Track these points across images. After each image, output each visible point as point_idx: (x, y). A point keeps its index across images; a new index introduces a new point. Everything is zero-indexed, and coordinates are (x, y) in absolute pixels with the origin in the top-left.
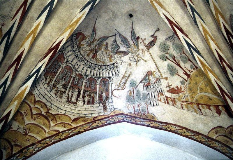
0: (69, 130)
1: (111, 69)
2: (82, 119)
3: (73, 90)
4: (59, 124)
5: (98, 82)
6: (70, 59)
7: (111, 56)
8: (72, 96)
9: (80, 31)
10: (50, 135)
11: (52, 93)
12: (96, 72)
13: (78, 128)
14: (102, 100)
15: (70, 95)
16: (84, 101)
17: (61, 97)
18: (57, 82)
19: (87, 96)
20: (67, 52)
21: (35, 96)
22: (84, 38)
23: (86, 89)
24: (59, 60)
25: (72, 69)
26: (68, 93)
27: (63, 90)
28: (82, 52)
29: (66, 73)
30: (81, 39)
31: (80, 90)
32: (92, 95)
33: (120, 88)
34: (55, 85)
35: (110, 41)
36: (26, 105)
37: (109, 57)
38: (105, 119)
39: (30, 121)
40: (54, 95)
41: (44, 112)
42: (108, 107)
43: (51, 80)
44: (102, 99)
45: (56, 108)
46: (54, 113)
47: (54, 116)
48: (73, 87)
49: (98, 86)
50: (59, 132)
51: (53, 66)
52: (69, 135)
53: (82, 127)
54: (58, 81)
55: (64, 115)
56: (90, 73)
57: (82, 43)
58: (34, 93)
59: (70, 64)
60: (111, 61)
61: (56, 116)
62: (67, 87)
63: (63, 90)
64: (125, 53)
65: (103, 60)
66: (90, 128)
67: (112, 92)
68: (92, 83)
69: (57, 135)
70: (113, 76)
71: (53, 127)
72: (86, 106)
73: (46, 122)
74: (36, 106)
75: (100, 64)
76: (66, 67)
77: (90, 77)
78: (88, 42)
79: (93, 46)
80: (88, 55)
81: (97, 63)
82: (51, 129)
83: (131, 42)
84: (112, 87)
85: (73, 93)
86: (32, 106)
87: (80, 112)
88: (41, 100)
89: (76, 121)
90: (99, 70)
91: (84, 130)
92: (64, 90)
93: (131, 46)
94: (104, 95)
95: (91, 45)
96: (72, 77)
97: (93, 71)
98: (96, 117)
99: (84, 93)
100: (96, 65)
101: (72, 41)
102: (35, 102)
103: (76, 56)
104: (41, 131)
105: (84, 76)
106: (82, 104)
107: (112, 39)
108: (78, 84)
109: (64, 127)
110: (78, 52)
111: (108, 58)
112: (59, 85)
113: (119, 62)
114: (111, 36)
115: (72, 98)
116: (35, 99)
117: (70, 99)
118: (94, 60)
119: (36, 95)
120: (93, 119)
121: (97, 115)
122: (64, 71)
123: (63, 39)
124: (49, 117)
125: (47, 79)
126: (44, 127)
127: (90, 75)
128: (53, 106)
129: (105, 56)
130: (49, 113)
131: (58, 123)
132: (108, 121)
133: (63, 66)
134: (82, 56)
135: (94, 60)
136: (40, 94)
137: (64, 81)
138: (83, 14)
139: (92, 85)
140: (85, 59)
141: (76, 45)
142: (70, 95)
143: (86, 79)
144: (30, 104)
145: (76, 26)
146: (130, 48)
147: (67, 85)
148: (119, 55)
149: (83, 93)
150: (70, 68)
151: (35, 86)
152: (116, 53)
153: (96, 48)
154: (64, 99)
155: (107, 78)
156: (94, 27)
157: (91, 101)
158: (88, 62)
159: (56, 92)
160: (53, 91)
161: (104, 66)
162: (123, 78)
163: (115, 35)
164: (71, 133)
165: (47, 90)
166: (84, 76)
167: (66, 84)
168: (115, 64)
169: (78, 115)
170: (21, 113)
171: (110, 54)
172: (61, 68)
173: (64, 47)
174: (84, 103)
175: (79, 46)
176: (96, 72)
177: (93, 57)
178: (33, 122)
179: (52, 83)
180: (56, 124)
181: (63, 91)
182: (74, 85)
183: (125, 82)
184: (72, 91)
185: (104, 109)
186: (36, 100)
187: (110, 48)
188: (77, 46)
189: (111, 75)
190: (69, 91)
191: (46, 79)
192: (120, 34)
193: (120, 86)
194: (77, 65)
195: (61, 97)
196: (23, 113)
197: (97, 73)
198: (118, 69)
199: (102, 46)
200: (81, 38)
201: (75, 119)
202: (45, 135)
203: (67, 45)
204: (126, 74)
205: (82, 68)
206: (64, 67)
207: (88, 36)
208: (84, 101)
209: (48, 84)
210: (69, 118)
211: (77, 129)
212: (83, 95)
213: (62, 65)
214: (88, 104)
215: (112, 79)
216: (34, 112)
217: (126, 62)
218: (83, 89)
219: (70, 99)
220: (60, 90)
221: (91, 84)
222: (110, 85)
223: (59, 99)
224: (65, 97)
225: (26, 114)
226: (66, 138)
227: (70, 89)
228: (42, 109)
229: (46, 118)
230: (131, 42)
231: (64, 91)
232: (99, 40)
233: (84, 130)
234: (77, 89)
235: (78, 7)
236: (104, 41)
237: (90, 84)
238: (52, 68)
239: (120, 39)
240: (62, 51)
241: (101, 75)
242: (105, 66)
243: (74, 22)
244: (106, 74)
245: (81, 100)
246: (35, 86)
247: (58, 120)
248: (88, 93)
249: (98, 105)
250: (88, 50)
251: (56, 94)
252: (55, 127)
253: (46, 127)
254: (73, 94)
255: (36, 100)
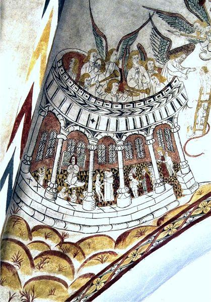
0: (112, 265)
1: (167, 98)
2: (134, 233)
3: (101, 176)
4: (90, 258)
5: (148, 138)
6: (72, 116)
7: (160, 69)
8: (103, 191)
9: (64, 52)
10: (77, 290)
11: (58, 201)
12: (137, 118)
13: (130, 255)
14: (168, 175)
15: (98, 190)
16: (130, 192)
17: (81, 201)
18: (63, 173)
19: (134, 177)
20: (58, 105)
21: (25, 222)
22: (82, 60)
23: (128, 163)
24: (49, 130)
25: (86, 135)
26: (93, 186)
27: (81, 184)
28: (92, 90)
29: (75, 148)
30: (77, 66)
31: (115, 170)
32: (144, 171)
33: (199, 133)
34: (60, 182)
35: (144, 38)
36: (13, 244)
37: (155, 75)
38: (182, 216)
39: (31, 274)
40: (65, 203)
41: (53, 245)
42: (183, 186)
43: (48, 175)
44: (167, 173)
45: (77, 228)
46: (75, 241)
47: (76, 245)
48: (99, 171)
49: (151, 148)
50: (93, 277)
51: (41, 147)
52: (113, 278)
53: (137, 250)
54: (65, 171)
55: (96, 236)
56: (127, 125)
57: (83, 72)
58: (22, 214)
59: (76, 125)
60: (162, 80)
61: (81, 245)
62: (87, 176)
63: (81, 184)
64: (187, 49)
65: (145, 85)
66: (152, 248)
67: (184, 149)
68: (137, 146)
69: (89, 284)
70: (175, 112)
71: (79, 270)
72: (138, 200)
73: (64, 263)
74: (34, 239)
75: (143, 96)
76: (71, 137)
77: (128, 135)
78: (95, 63)
79: (111, 67)
80: (108, 90)
81: (135, 99)
82: (76, 276)
83: (192, 18)
84: (182, 136)
85: (102, 182)
86: (26, 242)
87: (128, 219)
88: (42, 224)
89: (124, 240)
90: (144, 110)
91: (141, 256)
92: (84, 183)
93: (195, 26)
94: (169, 162)
95: (106, 67)
96: (90, 150)
97: (130, 119)
98: (162, 219)
99: (126, 173)
100: (133, 103)
101: (59, 78)
102: (31, 232)
103: (81, 104)
104: (59, 286)
105: (115, 138)
106: (129, 200)
107: (148, 29)
108: (107, 161)
109: (102, 262)
110: (81, 94)
111: (153, 77)
112: (70, 176)
113: (178, 74)
114: (141, 27)
115: (104, 194)
116: (28, 226)
117: (101, 198)
118: (125, 95)
119: (26, 217)
120: (158, 224)
121: (164, 211)
122: (68, 145)
123: (33, 86)
124: (68, 250)
125: (38, 177)
126: (61, 276)
127: (127, 129)
128: (69, 227)
129: (146, 74)
130: (66, 243)
131: (87, 257)
132: (188, 217)
133: (63, 136)
134: (96, 98)
135: (125, 95)
136: (36, 212)
137: (76, 166)
138: (51, 16)
139: (138, 150)
140: (103, 101)
141: (72, 83)
142: (98, 190)
143: (121, 143)
144: (21, 240)
145: (47, 48)
146: (193, 32)
147: (86, 172)
148: (177, 59)
149: (124, 174)
150: (79, 134)
151: (18, 201)
152: (168, 58)
153: (120, 66)
154: (89, 203)
155: (166, 122)
156: (95, 27)
157: (145, 186)
158: (114, 106)
159: (66, 195)
160: (62, 194)
161: (151, 97)
162: (199, 106)
163: (150, 19)
164: (116, 270)
165: (47, 199)
166: (115, 138)
167: (82, 170)
168: (173, 83)
169: (125, 226)
170: (8, 265)
171: (155, 67)
172: (60, 141)
173: (45, 99)
174: (132, 196)
175: (79, 82)
176: (137, 118)
177: (121, 90)
178: (37, 273)
179: (53, 180)
180: (85, 262)
181: (81, 188)
182: (100, 164)
183: (205, 115)
184: (100, 180)
185: (176, 192)
186: (31, 227)
187: (150, 53)
188: (76, 84)
189: (171, 112)
190: (95, 182)
191: (37, 177)
192: (159, 12)
193: (197, 128)
194: (93, 121)
195: (80, 202)
196: (12, 263)
197: (141, 121)
198: (183, 92)
199: (131, 57)
200: (75, 64)
201: (120, 237)
202: (66, 292)
203: (51, 92)
204: (202, 96)
205: (105, 124)
206: (65, 139)
207: (90, 52)
208: (130, 192)
209: (45, 185)
210: (108, 239)
211: (128, 257)
212: (125, 180)
213: (59, 136)
214: (139, 195)
215: (175, 120)
216: (35, 253)
217: (195, 69)
218: (121, 166)
219: (101, 198)
220: (74, 186)
221: (136, 149)
222: (176, 135)
223: (78, 207)
224: (89, 199)
225: (20, 263)
226: (108, 285)
227: (95, 178)
228: (48, 241)
229: (62, 255)
230: (192, 18)
231: (84, 186)
232: (118, 47)
233: (141, 256)
234: (109, 171)
235: (38, 4)
236: (132, 44)
237: (134, 149)
238: (41, 151)
239: (164, 22)
240: (47, 108)
241: (152, 121)
242: (153, 97)
243: (41, 41)
244: (158, 114)
245: (123, 191)
246: (18, 201)
247: (86, 251)
248: (134, 171)
249: (162, 188)
250: (104, 80)
251: (68, 199)
252: (83, 268)
253: (66, 274)
254: (103, 186)
255: (31, 227)
